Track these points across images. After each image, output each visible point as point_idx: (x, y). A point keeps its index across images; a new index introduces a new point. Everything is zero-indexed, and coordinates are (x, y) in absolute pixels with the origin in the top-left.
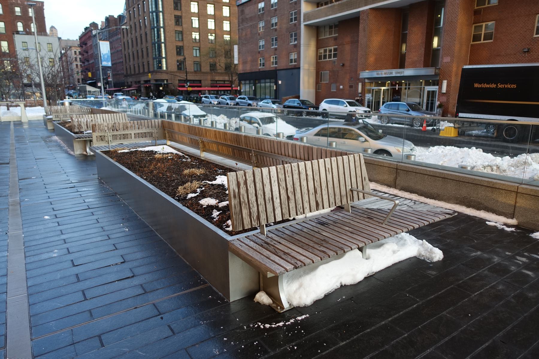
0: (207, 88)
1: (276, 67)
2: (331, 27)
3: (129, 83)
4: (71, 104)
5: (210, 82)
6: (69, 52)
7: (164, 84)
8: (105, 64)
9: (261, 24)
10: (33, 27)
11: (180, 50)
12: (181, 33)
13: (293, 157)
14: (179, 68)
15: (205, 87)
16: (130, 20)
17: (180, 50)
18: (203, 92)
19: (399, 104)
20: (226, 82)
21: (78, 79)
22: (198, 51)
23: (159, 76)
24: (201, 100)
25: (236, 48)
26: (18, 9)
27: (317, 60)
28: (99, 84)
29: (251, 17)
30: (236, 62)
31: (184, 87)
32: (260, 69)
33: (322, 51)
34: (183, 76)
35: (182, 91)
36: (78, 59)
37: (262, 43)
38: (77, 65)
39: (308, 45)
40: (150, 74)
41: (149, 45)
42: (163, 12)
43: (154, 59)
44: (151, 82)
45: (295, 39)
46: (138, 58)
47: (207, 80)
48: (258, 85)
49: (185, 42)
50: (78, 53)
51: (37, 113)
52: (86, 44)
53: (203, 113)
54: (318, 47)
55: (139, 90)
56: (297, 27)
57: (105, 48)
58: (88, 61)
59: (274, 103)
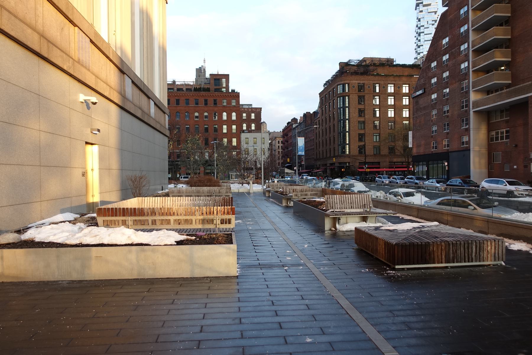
1: (448, 150)
2: (502, 112)
4: (278, 182)
6: (274, 142)
7: (347, 166)
8: (300, 153)
9: (434, 112)
10: (253, 127)
11: (361, 137)
12: (364, 122)
14: (360, 152)
16: (322, 115)
17: (362, 137)
18: (381, 173)
20: (404, 164)
21: (279, 163)
22: (378, 137)
23: (342, 160)
24: (375, 180)
25: (410, 133)
26: (244, 115)
27: (488, 141)
28: (295, 168)
29: (424, 107)
30: (410, 146)
31: (363, 168)
32: (432, 152)
33: (494, 133)
35: (361, 172)
36: (280, 147)
37: (435, 128)
38: (279, 152)
39: (478, 129)
41: (336, 134)
42: (349, 107)
43: (339, 145)
45: (467, 124)
46: (326, 145)
47: (385, 162)
48: (431, 166)
49: (366, 130)
50: (280, 142)
51: (257, 188)
52: (287, 135)
54: (489, 130)
55: (325, 171)
56: (467, 113)
57: (301, 142)
58: (288, 148)
59: (438, 182)
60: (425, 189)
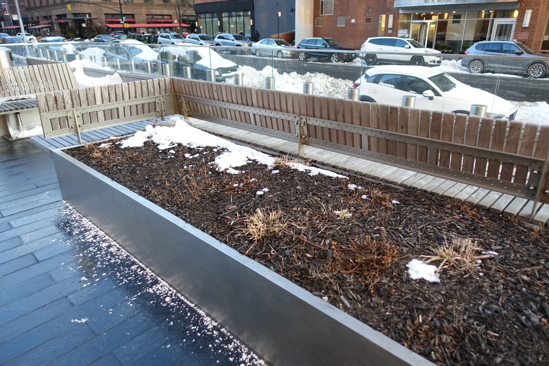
0: (142, 25)
3: (35, 19)
5: (146, 17)
13: (243, 104)
15: (140, 22)
19: (317, 40)
20: (165, 17)
31: (119, 23)
34: (117, 9)
40: (69, 5)
44: (68, 17)
53: (231, 64)
60: (254, 54)
